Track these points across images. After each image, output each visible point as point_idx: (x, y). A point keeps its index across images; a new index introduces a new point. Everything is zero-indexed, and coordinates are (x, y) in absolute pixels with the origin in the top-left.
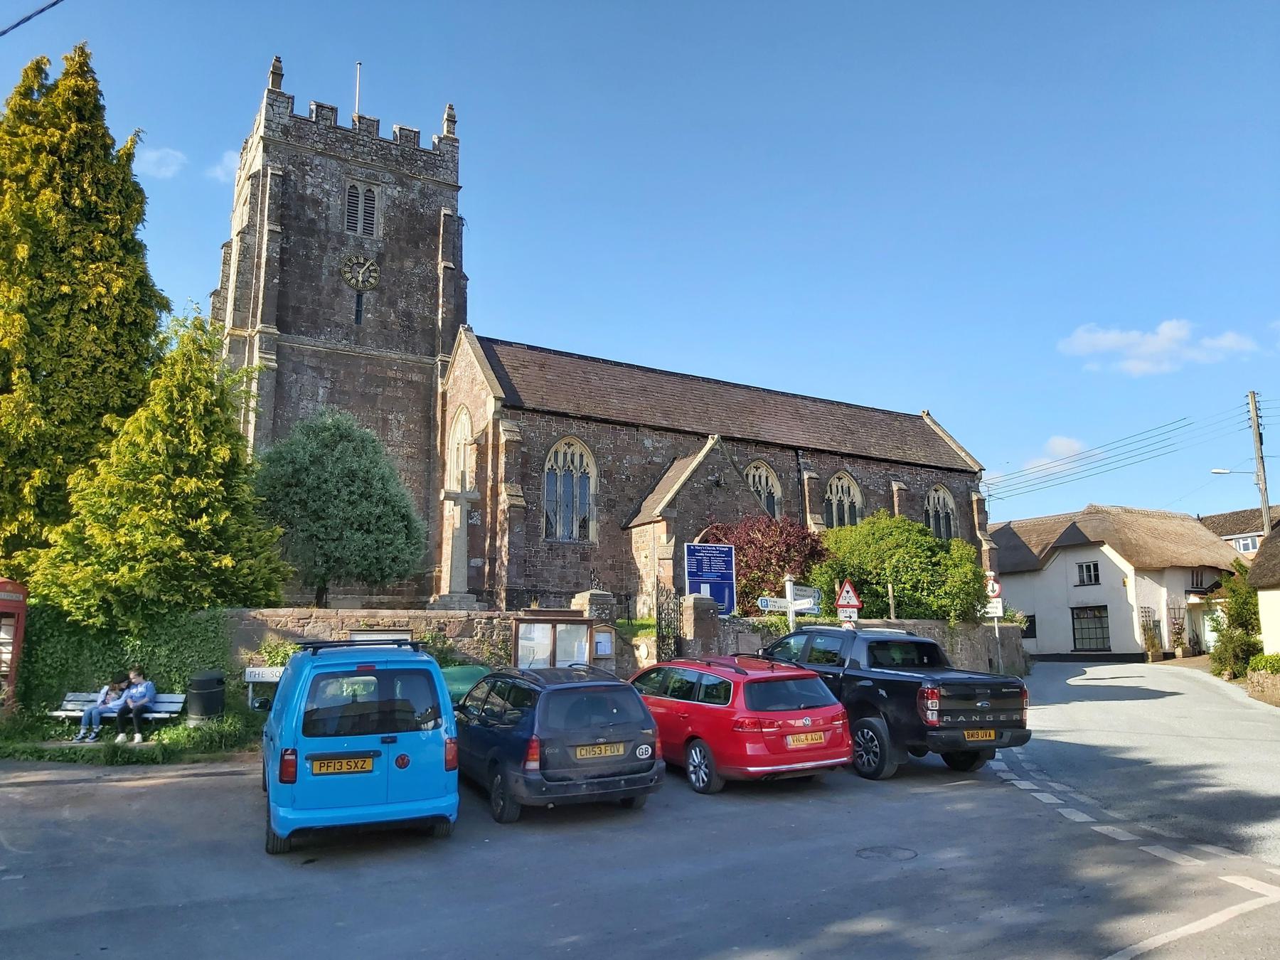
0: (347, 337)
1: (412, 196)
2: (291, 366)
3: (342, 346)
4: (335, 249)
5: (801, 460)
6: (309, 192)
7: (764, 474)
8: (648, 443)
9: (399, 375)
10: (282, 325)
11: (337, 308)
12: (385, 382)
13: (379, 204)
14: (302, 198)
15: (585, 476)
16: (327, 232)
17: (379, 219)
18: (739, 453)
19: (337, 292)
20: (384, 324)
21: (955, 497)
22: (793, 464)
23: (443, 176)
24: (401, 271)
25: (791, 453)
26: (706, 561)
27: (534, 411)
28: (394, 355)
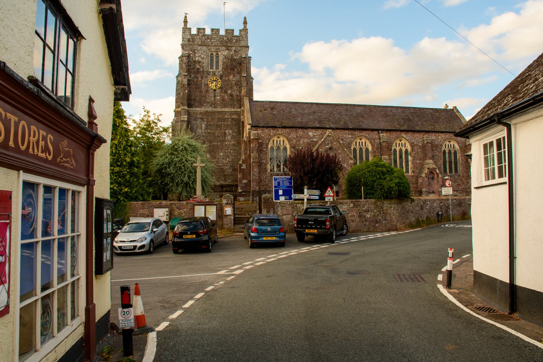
0: (211, 106)
1: (232, 53)
2: (193, 118)
3: (210, 109)
4: (206, 77)
5: (381, 135)
6: (197, 59)
7: (364, 142)
8: (311, 134)
9: (229, 117)
10: (189, 106)
11: (207, 97)
12: (224, 120)
13: (221, 58)
14: (195, 62)
15: (285, 148)
16: (203, 71)
17: (220, 63)
18: (352, 134)
19: (207, 91)
20: (223, 100)
21: (458, 144)
22: (377, 137)
23: (242, 43)
24: (229, 80)
25: (376, 132)
26: (281, 183)
27: (263, 127)
28: (226, 110)
